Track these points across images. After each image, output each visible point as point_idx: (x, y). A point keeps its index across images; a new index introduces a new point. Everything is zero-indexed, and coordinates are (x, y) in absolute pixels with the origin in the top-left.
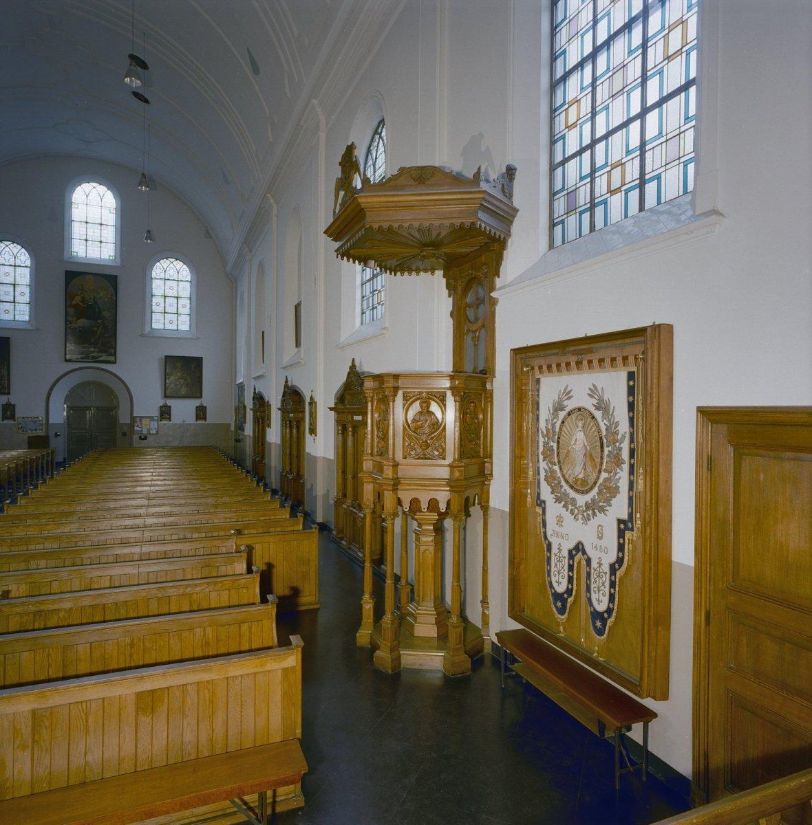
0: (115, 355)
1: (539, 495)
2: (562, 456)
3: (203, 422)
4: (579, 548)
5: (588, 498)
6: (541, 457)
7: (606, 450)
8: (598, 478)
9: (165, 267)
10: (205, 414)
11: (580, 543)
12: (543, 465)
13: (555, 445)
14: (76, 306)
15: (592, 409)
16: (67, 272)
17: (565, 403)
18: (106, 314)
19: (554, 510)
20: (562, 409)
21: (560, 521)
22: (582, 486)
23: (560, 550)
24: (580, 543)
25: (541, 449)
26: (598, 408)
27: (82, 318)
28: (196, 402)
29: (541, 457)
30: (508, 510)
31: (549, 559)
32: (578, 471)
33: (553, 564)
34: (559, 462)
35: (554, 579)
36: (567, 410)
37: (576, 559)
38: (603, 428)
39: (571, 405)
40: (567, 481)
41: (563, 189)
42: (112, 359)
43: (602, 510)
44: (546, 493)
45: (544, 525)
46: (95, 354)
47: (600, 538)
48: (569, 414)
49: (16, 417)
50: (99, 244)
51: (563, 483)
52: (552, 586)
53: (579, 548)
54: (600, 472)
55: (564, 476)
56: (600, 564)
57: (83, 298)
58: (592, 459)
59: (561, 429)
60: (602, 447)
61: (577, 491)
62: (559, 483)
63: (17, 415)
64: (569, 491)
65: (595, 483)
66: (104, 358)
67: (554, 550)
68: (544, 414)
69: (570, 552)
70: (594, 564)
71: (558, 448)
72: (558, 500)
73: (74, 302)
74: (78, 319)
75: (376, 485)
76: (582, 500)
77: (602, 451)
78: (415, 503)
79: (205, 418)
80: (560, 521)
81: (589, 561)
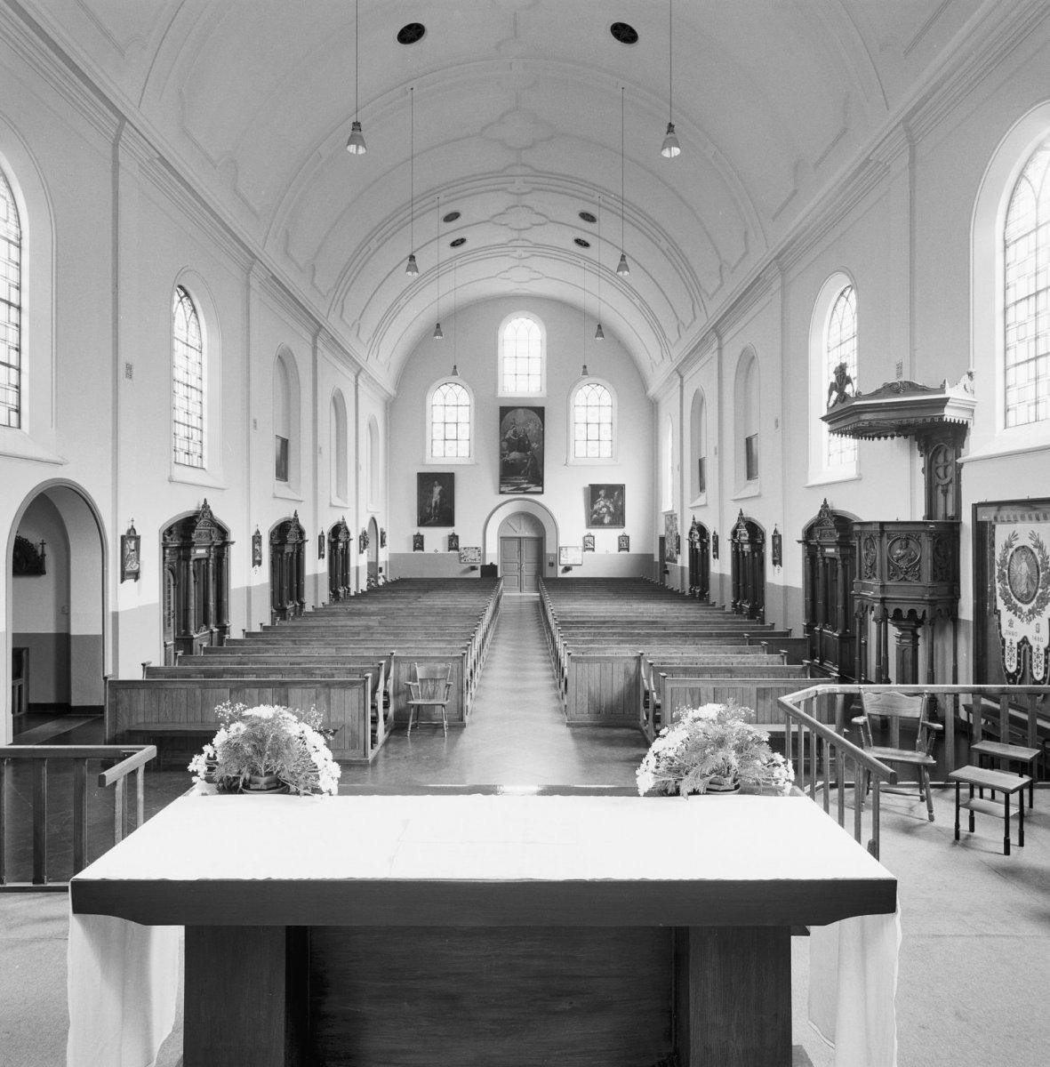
0: (542, 486)
1: (996, 607)
2: (1012, 578)
3: (421, 552)
4: (1025, 641)
5: (1030, 606)
6: (997, 580)
7: (1041, 574)
8: (1036, 593)
9: (587, 393)
10: (422, 543)
11: (1025, 637)
12: (998, 585)
13: (1006, 571)
14: (508, 440)
15: (1032, 547)
16: (501, 408)
17: (1014, 543)
18: (534, 445)
19: (1006, 616)
20: (1011, 547)
21: (1011, 624)
22: (1026, 599)
23: (1011, 643)
24: (1025, 637)
25: (997, 574)
26: (1035, 547)
27: (514, 450)
28: (447, 531)
29: (997, 580)
30: (971, 619)
31: (1004, 650)
32: (1023, 589)
33: (1006, 653)
34: (1010, 582)
35: (1007, 664)
36: (1015, 547)
37: (1023, 648)
38: (1039, 560)
39: (1017, 544)
40: (1015, 596)
41: (1029, 278)
42: (539, 489)
43: (1039, 613)
44: (1001, 605)
45: (1000, 627)
46: (525, 486)
47: (1038, 632)
48: (1016, 550)
49: (460, 547)
50: (527, 377)
51: (1013, 597)
52: (1006, 669)
53: (1025, 641)
54: (1037, 588)
55: (1013, 592)
56: (1038, 649)
57: (515, 432)
58: (1032, 580)
59: (1010, 560)
60: (1038, 572)
61: (1022, 602)
62: (1010, 597)
63: (461, 545)
64: (1017, 602)
65: (1034, 596)
66: (534, 489)
67: (1007, 644)
68: (998, 550)
69: (1018, 643)
70: (1034, 650)
71: (1009, 573)
72: (1009, 609)
73: (507, 436)
74: (511, 452)
75: (621, 708)
76: (1026, 608)
77: (1039, 575)
78: (898, 611)
79: (422, 548)
80: (1011, 624)
81: (1031, 648)
